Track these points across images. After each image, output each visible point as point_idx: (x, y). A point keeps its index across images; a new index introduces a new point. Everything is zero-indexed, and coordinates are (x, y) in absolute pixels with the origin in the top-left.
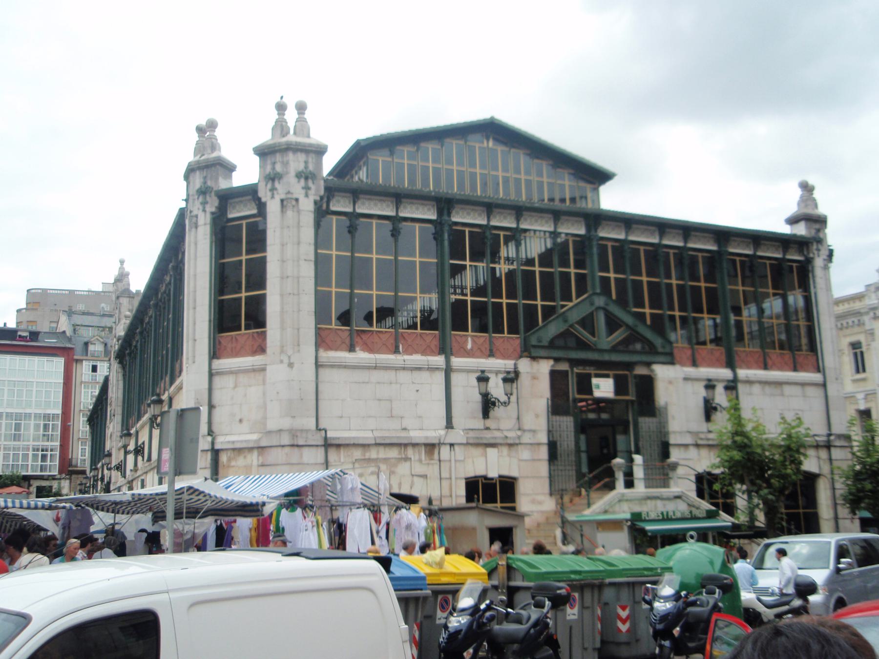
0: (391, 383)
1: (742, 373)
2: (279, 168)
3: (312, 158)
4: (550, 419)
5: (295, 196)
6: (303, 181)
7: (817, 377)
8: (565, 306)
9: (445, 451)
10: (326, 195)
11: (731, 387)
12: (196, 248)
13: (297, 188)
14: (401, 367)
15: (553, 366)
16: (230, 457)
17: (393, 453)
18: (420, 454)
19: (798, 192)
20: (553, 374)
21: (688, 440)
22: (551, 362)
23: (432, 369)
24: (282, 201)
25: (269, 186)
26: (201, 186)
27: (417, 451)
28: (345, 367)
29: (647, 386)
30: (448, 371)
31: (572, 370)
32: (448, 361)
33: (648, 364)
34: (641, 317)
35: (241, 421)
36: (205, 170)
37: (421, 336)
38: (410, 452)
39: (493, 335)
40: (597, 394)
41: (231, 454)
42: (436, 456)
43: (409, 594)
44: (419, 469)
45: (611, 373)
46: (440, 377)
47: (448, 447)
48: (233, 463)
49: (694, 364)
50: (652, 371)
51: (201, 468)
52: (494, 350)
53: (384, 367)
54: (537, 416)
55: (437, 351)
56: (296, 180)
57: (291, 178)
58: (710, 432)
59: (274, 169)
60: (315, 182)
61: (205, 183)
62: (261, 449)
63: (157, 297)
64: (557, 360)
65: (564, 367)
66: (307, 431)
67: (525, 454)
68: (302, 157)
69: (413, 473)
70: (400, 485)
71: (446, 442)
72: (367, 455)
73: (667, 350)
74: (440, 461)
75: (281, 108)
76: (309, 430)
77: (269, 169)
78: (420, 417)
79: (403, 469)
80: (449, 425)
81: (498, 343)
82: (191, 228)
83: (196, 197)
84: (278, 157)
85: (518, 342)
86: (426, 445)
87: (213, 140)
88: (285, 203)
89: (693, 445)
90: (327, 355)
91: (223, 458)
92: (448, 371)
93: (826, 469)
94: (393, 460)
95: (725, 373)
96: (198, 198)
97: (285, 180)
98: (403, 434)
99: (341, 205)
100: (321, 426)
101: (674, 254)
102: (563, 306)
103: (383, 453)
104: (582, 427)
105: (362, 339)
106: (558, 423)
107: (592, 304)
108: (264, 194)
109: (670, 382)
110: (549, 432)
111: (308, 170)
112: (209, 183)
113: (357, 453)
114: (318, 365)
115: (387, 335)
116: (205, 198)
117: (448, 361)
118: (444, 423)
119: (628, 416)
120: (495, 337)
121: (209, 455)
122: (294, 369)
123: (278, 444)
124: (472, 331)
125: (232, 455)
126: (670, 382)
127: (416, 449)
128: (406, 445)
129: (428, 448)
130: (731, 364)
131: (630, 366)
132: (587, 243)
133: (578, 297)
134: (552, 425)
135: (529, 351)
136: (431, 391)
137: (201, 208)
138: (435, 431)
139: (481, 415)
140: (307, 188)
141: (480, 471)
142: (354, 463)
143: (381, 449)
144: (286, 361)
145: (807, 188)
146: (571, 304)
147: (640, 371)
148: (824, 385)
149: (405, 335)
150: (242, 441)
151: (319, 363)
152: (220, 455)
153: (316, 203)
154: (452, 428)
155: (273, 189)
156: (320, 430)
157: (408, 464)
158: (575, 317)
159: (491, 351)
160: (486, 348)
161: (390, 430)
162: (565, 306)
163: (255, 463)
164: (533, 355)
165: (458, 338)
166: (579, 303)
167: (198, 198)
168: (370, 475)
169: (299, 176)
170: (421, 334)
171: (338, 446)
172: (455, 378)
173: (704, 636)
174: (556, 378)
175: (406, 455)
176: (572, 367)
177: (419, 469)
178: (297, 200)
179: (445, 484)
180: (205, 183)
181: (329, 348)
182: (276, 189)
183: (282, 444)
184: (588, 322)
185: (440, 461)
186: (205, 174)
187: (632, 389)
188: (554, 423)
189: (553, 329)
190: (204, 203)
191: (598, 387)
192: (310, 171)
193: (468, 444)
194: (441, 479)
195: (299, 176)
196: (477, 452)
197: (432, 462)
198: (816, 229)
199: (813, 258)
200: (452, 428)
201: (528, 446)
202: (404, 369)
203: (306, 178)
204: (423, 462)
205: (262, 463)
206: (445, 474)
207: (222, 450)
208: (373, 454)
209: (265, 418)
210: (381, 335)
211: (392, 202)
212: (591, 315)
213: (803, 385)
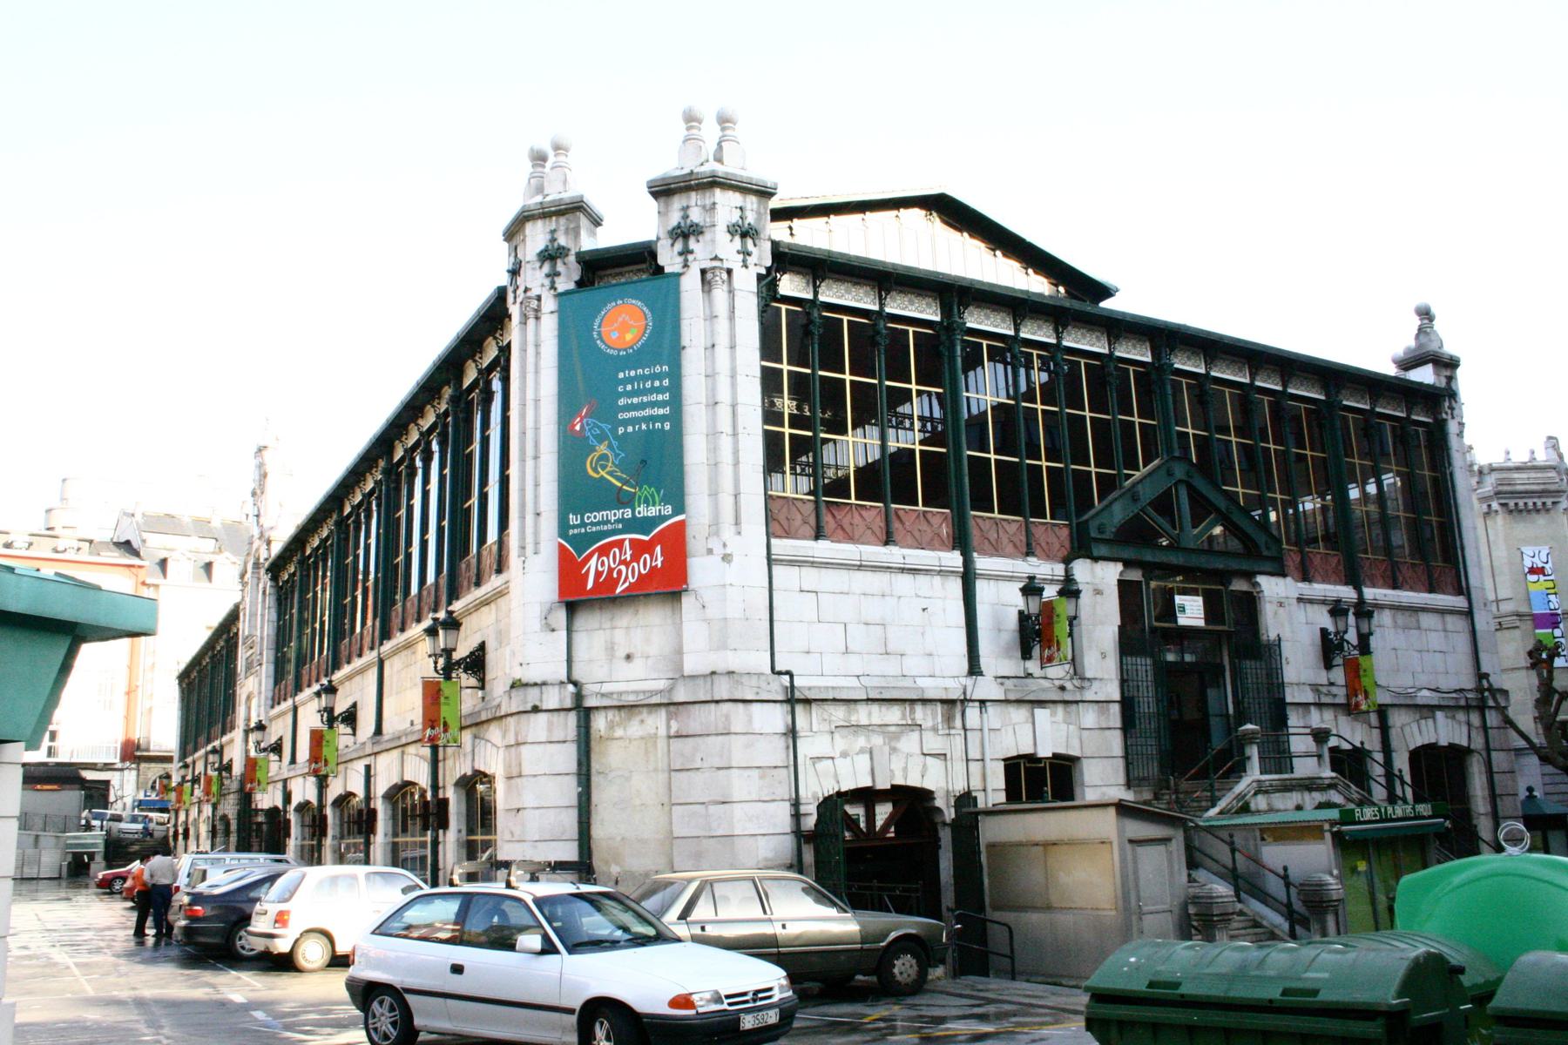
0: (883, 595)
1: (1370, 593)
2: (696, 216)
3: (752, 203)
4: (1124, 662)
5: (726, 265)
6: (737, 239)
7: (1459, 602)
8: (1130, 476)
9: (973, 713)
10: (775, 265)
11: (1364, 611)
12: (538, 354)
13: (728, 249)
14: (900, 568)
15: (1121, 574)
16: (612, 721)
17: (894, 715)
18: (934, 717)
19: (1416, 322)
20: (1123, 584)
21: (1309, 697)
22: (1119, 567)
23: (943, 573)
24: (703, 272)
25: (679, 246)
26: (547, 246)
27: (929, 712)
28: (813, 564)
29: (1250, 604)
30: (968, 579)
31: (1148, 585)
32: (968, 563)
33: (1249, 576)
34: (1232, 497)
35: (628, 657)
36: (554, 218)
37: (924, 516)
38: (920, 713)
39: (1032, 520)
40: (1182, 621)
41: (614, 716)
42: (958, 722)
43: (1163, 994)
44: (934, 743)
45: (1200, 587)
46: (956, 586)
47: (977, 704)
48: (619, 733)
49: (1306, 577)
50: (1256, 584)
51: (992, 760)
52: (1034, 544)
53: (872, 567)
54: (1104, 655)
55: (949, 542)
56: (729, 237)
57: (721, 235)
58: (1332, 684)
59: (686, 217)
60: (757, 241)
61: (553, 240)
62: (673, 706)
63: (392, 458)
64: (1128, 564)
65: (1135, 575)
66: (760, 674)
67: (1089, 717)
68: (735, 198)
69: (925, 752)
70: (905, 769)
71: (973, 698)
72: (854, 719)
73: (1273, 553)
74: (965, 729)
75: (691, 119)
76: (762, 674)
77: (675, 218)
78: (931, 655)
79: (910, 743)
80: (974, 669)
81: (1039, 532)
82: (524, 320)
83: (538, 265)
84: (694, 198)
85: (1065, 532)
86: (943, 702)
87: (566, 170)
88: (709, 276)
89: (1315, 704)
90: (781, 546)
91: (599, 723)
92: (968, 579)
93: (1478, 742)
94: (893, 729)
95: (1347, 593)
96: (541, 267)
97: (707, 236)
98: (908, 683)
99: (790, 285)
100: (576, 676)
101: (1269, 402)
102: (1129, 476)
103: (877, 715)
104: (1165, 674)
105: (834, 516)
106: (1134, 667)
107: (1170, 474)
108: (668, 258)
109: (1281, 604)
110: (1124, 683)
111: (747, 222)
112: (562, 240)
113: (838, 714)
114: (770, 561)
115: (874, 512)
116: (554, 266)
117: (968, 563)
118: (964, 665)
119: (1222, 659)
120: (1034, 522)
121: (572, 719)
122: (733, 564)
123: (709, 698)
124: (999, 513)
125: (617, 718)
126: (1281, 604)
127: (929, 708)
128: (912, 701)
129: (945, 706)
130: (1354, 580)
131: (1224, 577)
132: (1154, 376)
133: (1144, 466)
134: (1127, 670)
135: (1082, 547)
136: (944, 610)
137: (547, 282)
138: (948, 675)
139: (1019, 654)
140: (746, 253)
141: (1027, 749)
142: (832, 733)
143: (875, 708)
144: (719, 550)
145: (1425, 314)
146: (1137, 474)
147: (1239, 585)
148: (1469, 614)
149: (901, 513)
150: (636, 692)
151: (773, 557)
152: (592, 716)
153: (760, 277)
154: (981, 674)
155: (686, 252)
156: (780, 673)
157: (915, 735)
158: (1148, 493)
159: (1028, 545)
160: (1021, 541)
161: (881, 673)
162: (1130, 476)
163: (662, 732)
164: (1096, 553)
165: (979, 521)
166: (1150, 474)
167: (541, 267)
168: (857, 754)
169: (733, 230)
170: (925, 513)
171: (807, 702)
172: (982, 589)
173: (232, 846)
174: (1126, 590)
175: (913, 719)
176: (1148, 578)
177: (934, 743)
178: (729, 272)
179: (975, 767)
180: (553, 240)
181: (788, 534)
182: (691, 252)
183: (716, 698)
184: (1163, 504)
185: (965, 729)
186: (553, 227)
187: (1229, 615)
188: (1129, 667)
189: (1119, 513)
190: (554, 274)
191: (1183, 609)
192: (749, 224)
193: (1007, 701)
194: (967, 760)
195: (733, 230)
196: (1019, 714)
197: (952, 732)
198: (1446, 377)
199: (1446, 420)
200: (981, 674)
201: (1095, 706)
202: (903, 570)
203: (744, 235)
204: (940, 732)
205: (677, 732)
206: (974, 753)
207: (597, 708)
208: (863, 715)
209: (679, 652)
210: (864, 513)
211: (873, 288)
212: (1168, 493)
213: (1442, 612)
